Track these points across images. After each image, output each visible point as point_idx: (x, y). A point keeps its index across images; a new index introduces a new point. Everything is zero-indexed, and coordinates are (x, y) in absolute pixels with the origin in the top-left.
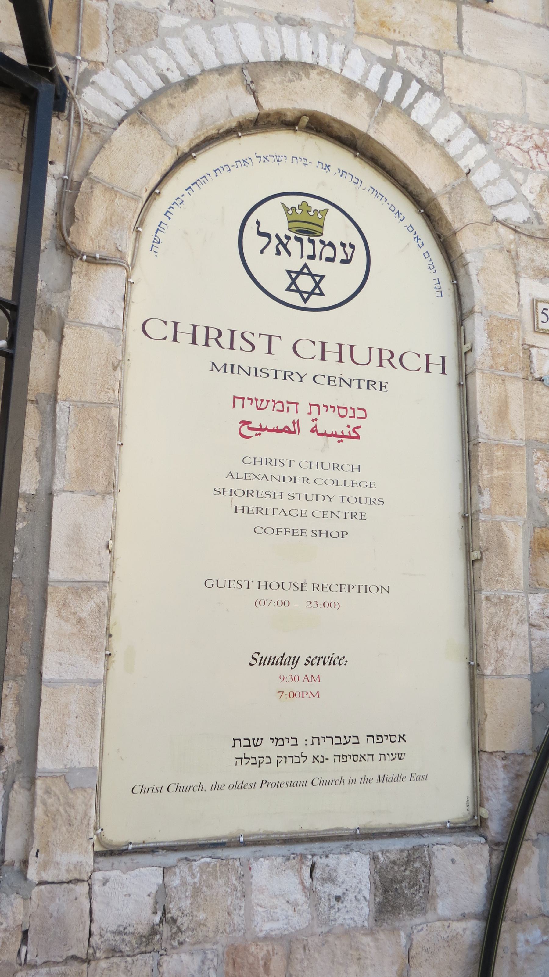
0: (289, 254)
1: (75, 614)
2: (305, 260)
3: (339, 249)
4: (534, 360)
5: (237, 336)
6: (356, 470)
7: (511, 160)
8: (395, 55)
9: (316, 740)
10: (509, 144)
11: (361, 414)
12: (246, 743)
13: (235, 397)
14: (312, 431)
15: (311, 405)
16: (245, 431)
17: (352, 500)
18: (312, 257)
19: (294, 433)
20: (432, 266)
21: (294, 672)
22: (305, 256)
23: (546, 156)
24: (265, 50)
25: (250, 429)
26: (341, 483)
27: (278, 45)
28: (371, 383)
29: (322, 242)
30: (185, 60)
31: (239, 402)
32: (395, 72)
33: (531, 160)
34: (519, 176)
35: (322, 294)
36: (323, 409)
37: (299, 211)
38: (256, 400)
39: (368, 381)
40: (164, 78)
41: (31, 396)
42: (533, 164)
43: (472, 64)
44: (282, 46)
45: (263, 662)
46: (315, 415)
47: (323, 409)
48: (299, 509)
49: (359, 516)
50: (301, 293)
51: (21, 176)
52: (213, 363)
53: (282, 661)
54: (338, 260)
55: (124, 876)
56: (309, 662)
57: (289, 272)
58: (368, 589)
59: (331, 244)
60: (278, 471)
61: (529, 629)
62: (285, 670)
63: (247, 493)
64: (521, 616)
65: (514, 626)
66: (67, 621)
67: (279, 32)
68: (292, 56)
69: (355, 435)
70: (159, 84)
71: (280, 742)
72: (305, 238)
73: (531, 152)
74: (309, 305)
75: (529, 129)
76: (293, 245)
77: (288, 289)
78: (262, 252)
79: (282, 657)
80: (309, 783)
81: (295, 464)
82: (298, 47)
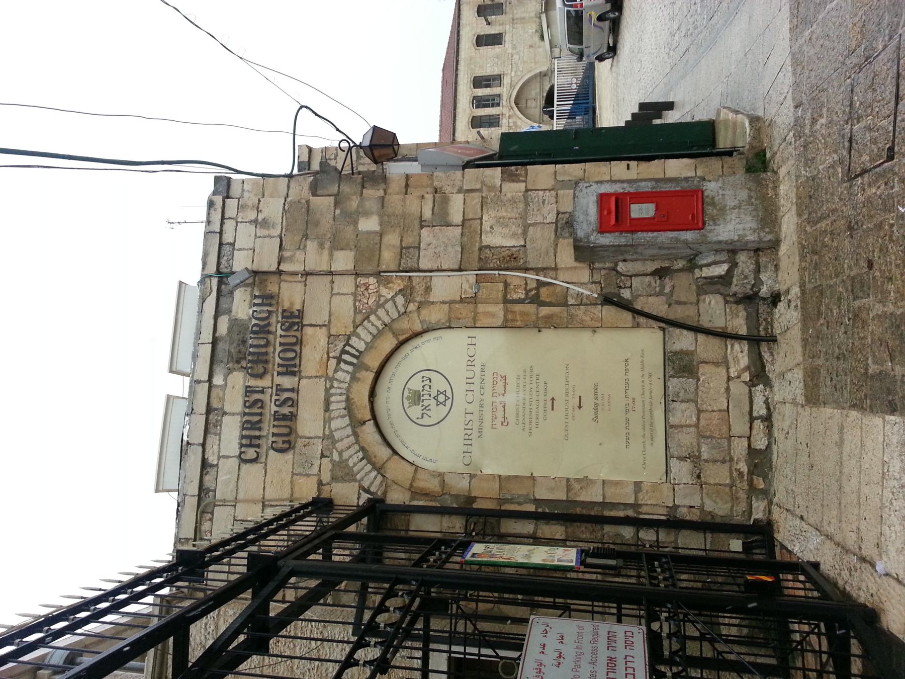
2: (432, 398)
3: (425, 383)
5: (467, 427)
8: (334, 358)
11: (495, 374)
16: (505, 424)
18: (430, 395)
20: (428, 341)
24: (343, 417)
27: (339, 411)
30: (352, 451)
34: (382, 299)
41: (498, 508)
45: (597, 417)
51: (412, 514)
53: (596, 409)
57: (437, 405)
58: (567, 373)
59: (423, 387)
60: (521, 410)
62: (599, 408)
63: (530, 423)
68: (343, 405)
70: (364, 461)
72: (422, 398)
74: (451, 397)
76: (426, 403)
82: (338, 402)
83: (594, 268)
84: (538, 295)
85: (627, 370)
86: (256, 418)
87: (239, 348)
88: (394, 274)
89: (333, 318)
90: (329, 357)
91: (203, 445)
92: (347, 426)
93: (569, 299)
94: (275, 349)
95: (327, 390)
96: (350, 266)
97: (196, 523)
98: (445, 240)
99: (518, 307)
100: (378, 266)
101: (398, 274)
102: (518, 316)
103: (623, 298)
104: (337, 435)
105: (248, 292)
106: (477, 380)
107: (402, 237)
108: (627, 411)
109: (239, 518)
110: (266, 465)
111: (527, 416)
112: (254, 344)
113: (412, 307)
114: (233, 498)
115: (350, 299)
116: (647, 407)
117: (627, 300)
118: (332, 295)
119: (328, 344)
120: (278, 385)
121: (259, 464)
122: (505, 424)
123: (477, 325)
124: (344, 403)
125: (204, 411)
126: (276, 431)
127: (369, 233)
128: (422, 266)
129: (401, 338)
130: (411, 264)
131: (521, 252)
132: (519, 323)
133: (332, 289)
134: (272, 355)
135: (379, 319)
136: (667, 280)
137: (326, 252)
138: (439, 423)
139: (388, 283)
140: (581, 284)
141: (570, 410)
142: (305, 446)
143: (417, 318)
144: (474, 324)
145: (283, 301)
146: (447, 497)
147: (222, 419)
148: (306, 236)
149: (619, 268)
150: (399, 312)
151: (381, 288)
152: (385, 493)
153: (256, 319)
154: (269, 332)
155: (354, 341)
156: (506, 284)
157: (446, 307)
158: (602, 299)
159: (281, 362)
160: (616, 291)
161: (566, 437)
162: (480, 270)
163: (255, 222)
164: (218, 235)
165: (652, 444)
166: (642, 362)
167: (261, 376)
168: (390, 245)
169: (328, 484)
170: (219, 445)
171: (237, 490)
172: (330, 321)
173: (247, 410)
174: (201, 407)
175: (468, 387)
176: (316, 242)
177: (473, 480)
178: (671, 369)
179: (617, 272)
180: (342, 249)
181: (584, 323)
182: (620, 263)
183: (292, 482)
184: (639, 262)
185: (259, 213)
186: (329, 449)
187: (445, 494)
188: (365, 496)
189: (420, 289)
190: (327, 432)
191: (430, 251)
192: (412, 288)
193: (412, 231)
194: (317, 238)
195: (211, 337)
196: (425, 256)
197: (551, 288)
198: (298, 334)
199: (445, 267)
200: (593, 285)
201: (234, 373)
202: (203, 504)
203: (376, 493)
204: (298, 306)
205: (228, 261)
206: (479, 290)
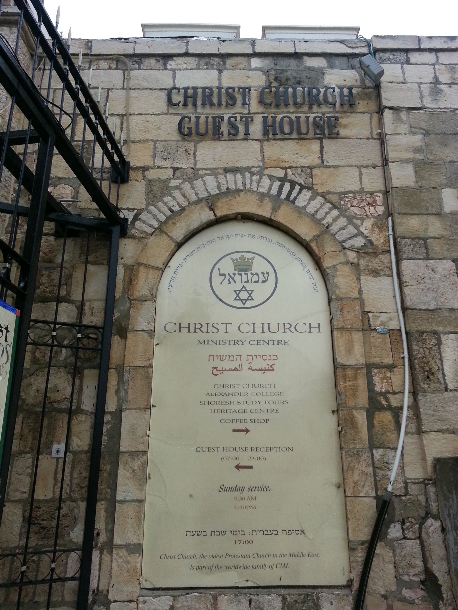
0: (235, 282)
1: (132, 467)
2: (243, 284)
3: (261, 276)
4: (371, 320)
5: (210, 326)
6: (273, 387)
7: (354, 214)
8: (286, 174)
9: (254, 532)
10: (352, 206)
11: (275, 357)
12: (218, 533)
13: (209, 356)
14: (249, 369)
15: (248, 356)
16: (215, 372)
17: (271, 402)
18: (246, 282)
19: (240, 370)
20: (311, 277)
21: (242, 495)
22: (243, 282)
23: (375, 208)
24: (219, 187)
25: (217, 371)
26: (265, 394)
27: (225, 183)
28: (279, 341)
29: (252, 274)
30: (181, 200)
31: (211, 358)
32: (286, 183)
33: (366, 212)
34: (358, 222)
35: (252, 299)
36: (254, 357)
37: (239, 260)
38: (220, 356)
39: (278, 341)
40: (172, 211)
41: (112, 366)
42: (367, 214)
43: (329, 169)
44: (227, 184)
45: (226, 490)
46: (250, 360)
47: (254, 357)
48: (243, 409)
49: (275, 411)
50: (242, 300)
52: (199, 340)
54: (260, 281)
55: (154, 600)
56: (250, 489)
57: (235, 291)
58: (281, 450)
59: (257, 274)
60: (231, 390)
61: (373, 469)
62: (237, 494)
63: (217, 403)
64: (368, 463)
65: (364, 468)
66: (128, 471)
67: (225, 176)
68: (232, 187)
69: (272, 369)
70: (169, 213)
71: (235, 533)
72: (243, 273)
73: (365, 208)
74: (246, 306)
75: (364, 196)
76: (237, 278)
77: (235, 299)
78: (221, 283)
79: (236, 487)
80: (251, 556)
81: (241, 387)
82: (235, 182)
83: (426, 485)
84: (381, 408)
85: (289, 532)
86: (215, 101)
87: (291, 78)
88: (391, 232)
89: (332, 170)
90: (286, 168)
91: (187, 54)
92: (208, 192)
93: (381, 451)
94: (292, 113)
95: (248, 169)
96: (396, 183)
97: (107, 55)
98: (441, 290)
99: (362, 383)
100: (399, 214)
101: (391, 237)
102: (351, 383)
103: (388, 527)
104: (198, 183)
105: (354, 83)
106: (267, 336)
107: (439, 238)
108: (234, 532)
109: (110, 93)
110: (166, 114)
111: (225, 398)
112: (298, 93)
113: (352, 256)
114: (131, 86)
115: (355, 187)
116: (243, 562)
117: (387, 534)
118: (359, 167)
119: (302, 167)
120: (252, 118)
121: (166, 108)
122: (215, 372)
123: (335, 333)
124: (234, 187)
125: (222, 51)
126: (202, 119)
127: (440, 201)
128: (405, 265)
129: (313, 245)
130: (406, 250)
131: (438, 385)
132: (341, 384)
133: (367, 167)
134: (286, 110)
135: (335, 220)
136: (421, 593)
137: (410, 155)
138: (221, 300)
139: (378, 227)
140: (402, 468)
141: (233, 454)
142: (186, 151)
143: (338, 261)
144: (337, 329)
145: (348, 117)
146: (128, 305)
147: (214, 69)
148: (427, 133)
149: (430, 521)
150: (344, 241)
151: (372, 220)
152: (133, 237)
153: (325, 92)
154: (311, 106)
155: (306, 194)
156: (391, 367)
157: (355, 294)
158: (386, 498)
159: (278, 119)
160: (397, 517)
161: (199, 450)
162: (407, 333)
163: (436, 82)
164: (418, 47)
165: (192, 568)
166: (302, 555)
167: (261, 102)
168: (427, 225)
169: (144, 177)
170: (187, 69)
171: (139, 89)
172: (328, 167)
173: (223, 91)
174: (225, 49)
175: (258, 325)
176: (421, 144)
177: (146, 335)
178: (296, 598)
179: (425, 519)
180: (416, 172)
181: (350, 472)
182: (437, 524)
183: (147, 140)
184: (443, 552)
185: (447, 86)
186: (182, 176)
187: (131, 303)
188: (130, 216)
189: (375, 263)
190: (201, 172)
191: (426, 273)
192: (375, 254)
193: (448, 250)
194: (427, 145)
195: (302, 51)
196: (418, 266)
197: (392, 426)
198: (311, 135)
199: (406, 290)
200: (402, 485)
201: (264, 76)
202: (126, 60)
203: (134, 228)
204: (343, 132)
205: (389, 59)
206: (380, 333)
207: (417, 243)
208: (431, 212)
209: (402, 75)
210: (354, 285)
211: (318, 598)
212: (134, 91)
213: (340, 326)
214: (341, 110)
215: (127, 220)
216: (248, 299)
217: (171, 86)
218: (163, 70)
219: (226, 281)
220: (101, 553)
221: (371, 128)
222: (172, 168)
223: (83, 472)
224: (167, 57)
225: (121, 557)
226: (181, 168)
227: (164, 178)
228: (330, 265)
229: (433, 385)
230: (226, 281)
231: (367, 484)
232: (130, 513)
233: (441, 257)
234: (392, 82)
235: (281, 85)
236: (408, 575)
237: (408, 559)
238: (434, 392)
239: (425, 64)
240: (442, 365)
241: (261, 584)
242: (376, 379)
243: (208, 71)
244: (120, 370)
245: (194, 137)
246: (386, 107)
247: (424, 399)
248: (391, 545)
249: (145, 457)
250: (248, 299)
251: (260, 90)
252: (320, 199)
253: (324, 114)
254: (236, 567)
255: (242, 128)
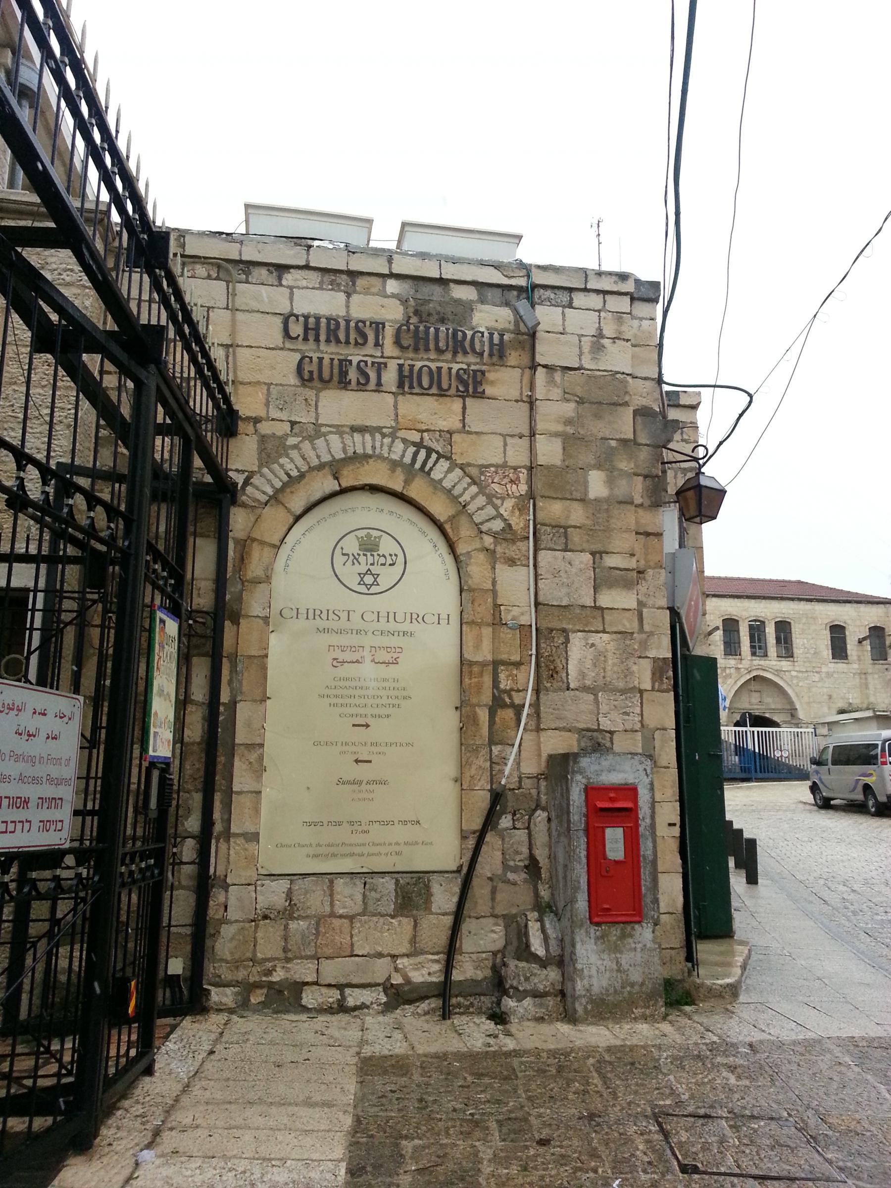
2: (369, 566)
3: (388, 558)
4: (503, 613)
5: (331, 612)
7: (494, 492)
8: (422, 439)
10: (493, 482)
11: (400, 650)
16: (335, 663)
18: (372, 564)
20: (444, 562)
24: (344, 450)
27: (352, 445)
29: (378, 555)
30: (300, 462)
41: (225, 654)
45: (343, 783)
54: (388, 563)
56: (368, 783)
58: (401, 745)
59: (384, 556)
60: (353, 684)
63: (336, 696)
67: (352, 437)
68: (360, 451)
70: (285, 478)
72: (369, 554)
74: (371, 591)
76: (362, 559)
77: (359, 584)
83: (539, 780)
84: (504, 706)
86: (342, 336)
87: (434, 313)
88: (532, 517)
89: (473, 437)
90: (422, 431)
91: (307, 267)
92: (332, 456)
93: (499, 747)
94: (433, 361)
95: (379, 429)
97: (205, 258)
99: (487, 680)
100: (542, 497)
101: (531, 522)
103: (500, 818)
104: (320, 442)
105: (507, 326)
106: (392, 626)
107: (579, 527)
108: (351, 823)
109: (211, 314)
110: (281, 349)
112: (440, 334)
113: (488, 541)
114: (237, 306)
115: (499, 460)
117: (498, 824)
118: (504, 436)
119: (440, 431)
120: (385, 364)
121: (281, 340)
122: (335, 663)
123: (464, 626)
125: (352, 267)
128: (542, 554)
129: (448, 527)
130: (545, 539)
132: (467, 681)
133: (512, 436)
134: (425, 357)
136: (523, 876)
137: (560, 428)
139: (519, 510)
140: (518, 763)
141: (353, 748)
142: (306, 400)
145: (496, 371)
146: (239, 586)
147: (341, 291)
148: (581, 402)
149: (539, 812)
150: (482, 523)
152: (244, 505)
153: (473, 337)
154: (455, 353)
155: (444, 465)
156: (518, 664)
158: (499, 790)
159: (416, 369)
162: (537, 629)
163: (600, 335)
164: (583, 287)
165: (308, 856)
166: (417, 843)
167: (397, 342)
168: (569, 511)
169: (256, 431)
171: (248, 311)
172: (469, 433)
173: (352, 324)
175: (383, 614)
176: (573, 415)
177: (261, 622)
179: (535, 810)
180: (564, 449)
181: (468, 767)
182: (546, 814)
185: (611, 341)
186: (301, 432)
188: (240, 479)
189: (512, 551)
190: (323, 429)
192: (513, 541)
193: (588, 541)
194: (579, 416)
195: (449, 277)
196: (555, 558)
197: (513, 724)
198: (453, 391)
199: (541, 584)
200: (517, 779)
201: (402, 307)
202: (229, 266)
203: (244, 494)
204: (489, 390)
205: (549, 299)
206: (510, 628)
207: (557, 532)
208: (574, 497)
209: (561, 323)
210: (488, 575)
211: (429, 881)
212: (241, 313)
213: (470, 620)
214: (489, 361)
215: (237, 484)
216: (373, 584)
217: (286, 310)
218: (277, 286)
219: (350, 562)
220: (217, 842)
221: (521, 388)
222: (290, 421)
223: (196, 763)
224: (282, 269)
225: (239, 845)
226: (300, 422)
227: (279, 433)
228: (464, 552)
229: (556, 685)
230: (350, 562)
231: (483, 778)
232: (248, 804)
233: (579, 549)
234: (548, 332)
235: (421, 322)
236: (514, 861)
237: (515, 847)
238: (555, 691)
239: (590, 310)
240: (567, 664)
241: (376, 871)
242: (502, 676)
243: (333, 292)
244: (234, 658)
245: (316, 383)
246: (539, 365)
247: (546, 698)
248: (501, 835)
249: (261, 750)
250: (373, 584)
251: (397, 326)
252: (458, 472)
253: (469, 365)
254: (352, 855)
255: (373, 375)
